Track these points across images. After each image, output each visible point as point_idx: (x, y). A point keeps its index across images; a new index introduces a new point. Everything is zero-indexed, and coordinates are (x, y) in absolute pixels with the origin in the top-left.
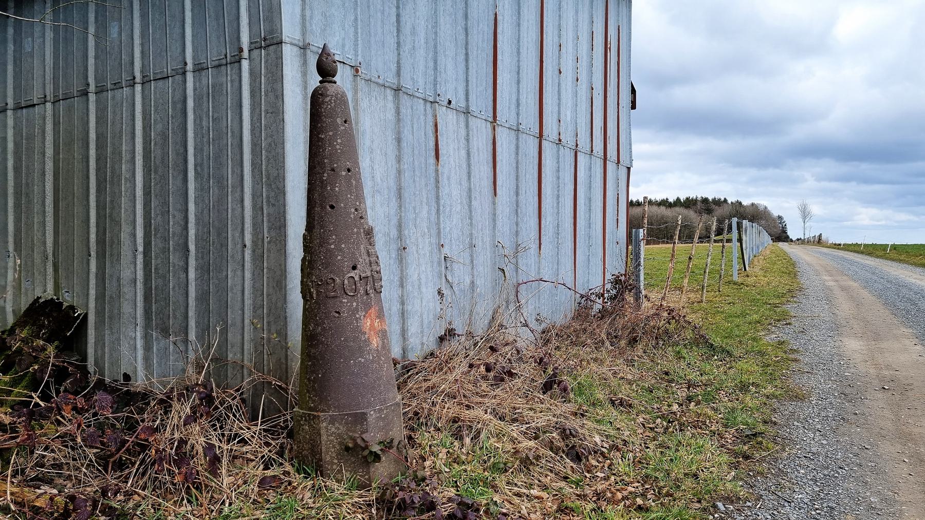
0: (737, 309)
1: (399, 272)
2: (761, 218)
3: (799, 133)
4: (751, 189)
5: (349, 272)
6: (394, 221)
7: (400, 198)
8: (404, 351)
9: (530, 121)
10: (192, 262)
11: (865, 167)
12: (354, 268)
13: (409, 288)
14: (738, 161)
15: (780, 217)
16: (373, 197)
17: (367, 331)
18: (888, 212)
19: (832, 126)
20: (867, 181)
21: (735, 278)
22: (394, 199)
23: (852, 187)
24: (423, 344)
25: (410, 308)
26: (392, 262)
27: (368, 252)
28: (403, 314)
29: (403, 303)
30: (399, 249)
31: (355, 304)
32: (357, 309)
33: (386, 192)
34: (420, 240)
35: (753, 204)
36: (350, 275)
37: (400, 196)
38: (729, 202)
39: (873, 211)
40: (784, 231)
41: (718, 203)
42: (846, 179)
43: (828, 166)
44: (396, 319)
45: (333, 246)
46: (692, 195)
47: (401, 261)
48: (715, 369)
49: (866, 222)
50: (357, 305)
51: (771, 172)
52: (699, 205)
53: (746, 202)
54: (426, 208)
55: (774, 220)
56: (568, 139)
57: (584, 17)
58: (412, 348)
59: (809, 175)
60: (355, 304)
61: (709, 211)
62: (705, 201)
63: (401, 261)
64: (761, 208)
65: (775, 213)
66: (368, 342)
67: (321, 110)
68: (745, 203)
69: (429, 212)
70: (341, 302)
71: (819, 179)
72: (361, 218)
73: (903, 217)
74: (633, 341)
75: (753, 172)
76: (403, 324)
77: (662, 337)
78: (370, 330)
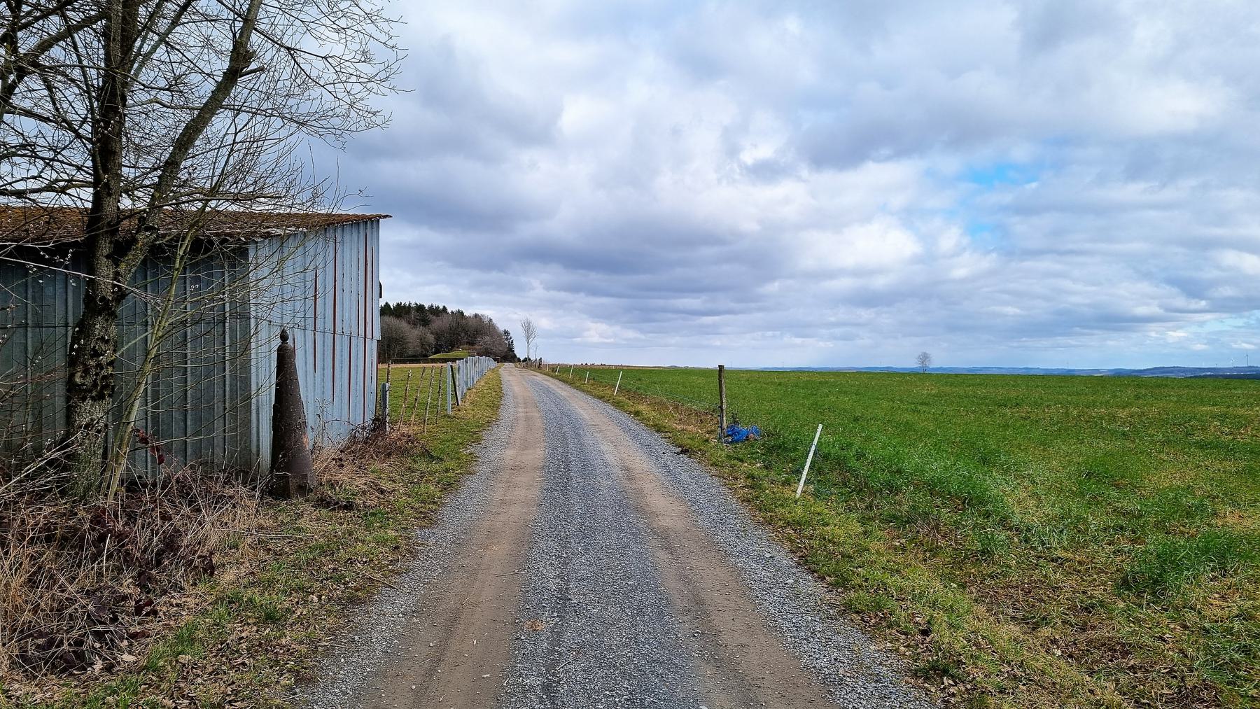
0: (449, 436)
2: (485, 334)
3: (527, 232)
4: (474, 296)
9: (330, 326)
10: (189, 417)
11: (595, 278)
14: (458, 260)
15: (506, 332)
18: (617, 329)
19: (561, 225)
20: (594, 292)
21: (449, 412)
23: (582, 299)
35: (476, 316)
38: (449, 311)
39: (602, 327)
40: (511, 349)
41: (438, 312)
42: (574, 289)
43: (554, 273)
46: (405, 301)
48: (435, 466)
49: (596, 339)
51: (494, 275)
52: (413, 314)
53: (468, 312)
55: (499, 335)
56: (347, 332)
57: (355, 250)
59: (537, 280)
61: (425, 323)
62: (420, 308)
64: (486, 321)
65: (501, 326)
67: (285, 359)
68: (467, 314)
71: (548, 288)
73: (631, 334)
74: (389, 455)
75: (477, 275)
77: (404, 452)
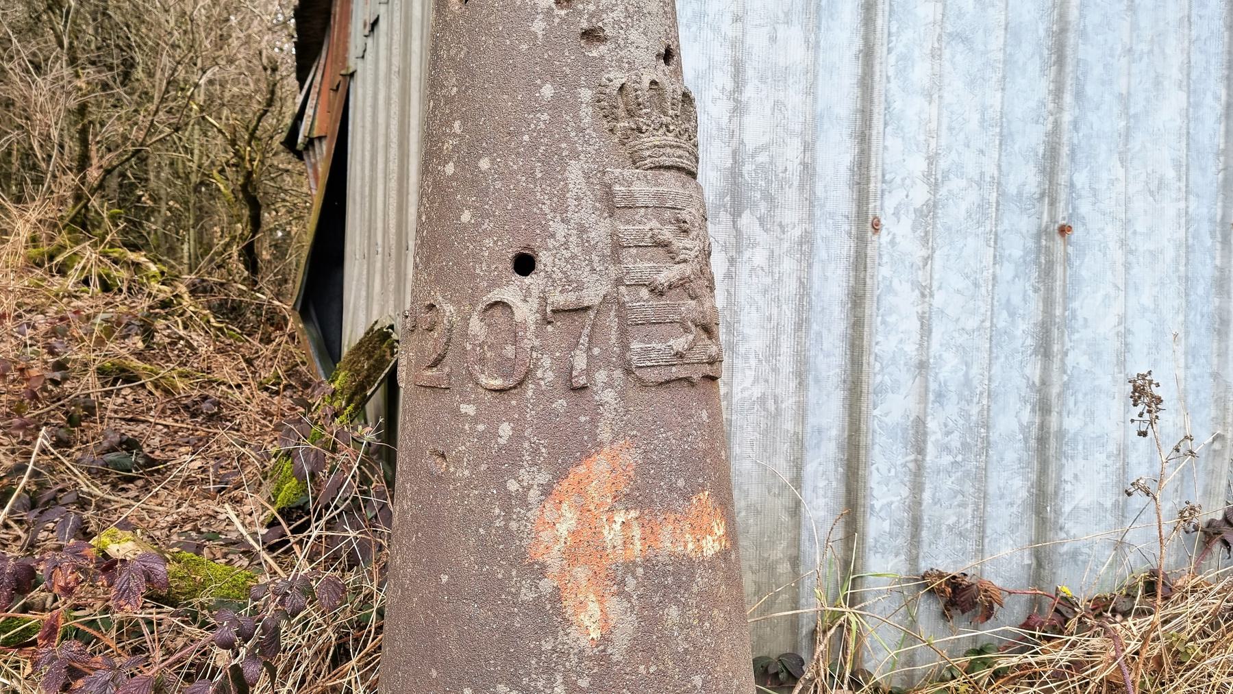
1: (1034, 309)
5: (494, 284)
6: (1033, 137)
7: (1060, 61)
8: (1041, 560)
12: (525, 264)
13: (1077, 359)
16: (936, 54)
17: (553, 560)
22: (1034, 67)
24: (1120, 545)
25: (1072, 424)
26: (1006, 272)
27: (609, 194)
28: (1042, 440)
29: (1044, 407)
30: (1041, 233)
31: (506, 430)
32: (510, 458)
33: (997, 40)
34: (1139, 205)
36: (495, 295)
37: (1059, 54)
44: (1011, 456)
45: (450, 169)
47: (1047, 273)
50: (518, 436)
54: (1175, 100)
58: (1074, 555)
60: (506, 430)
63: (1047, 273)
66: (551, 614)
69: (1191, 113)
70: (456, 413)
72: (591, 35)
76: (1043, 471)
78: (571, 556)
